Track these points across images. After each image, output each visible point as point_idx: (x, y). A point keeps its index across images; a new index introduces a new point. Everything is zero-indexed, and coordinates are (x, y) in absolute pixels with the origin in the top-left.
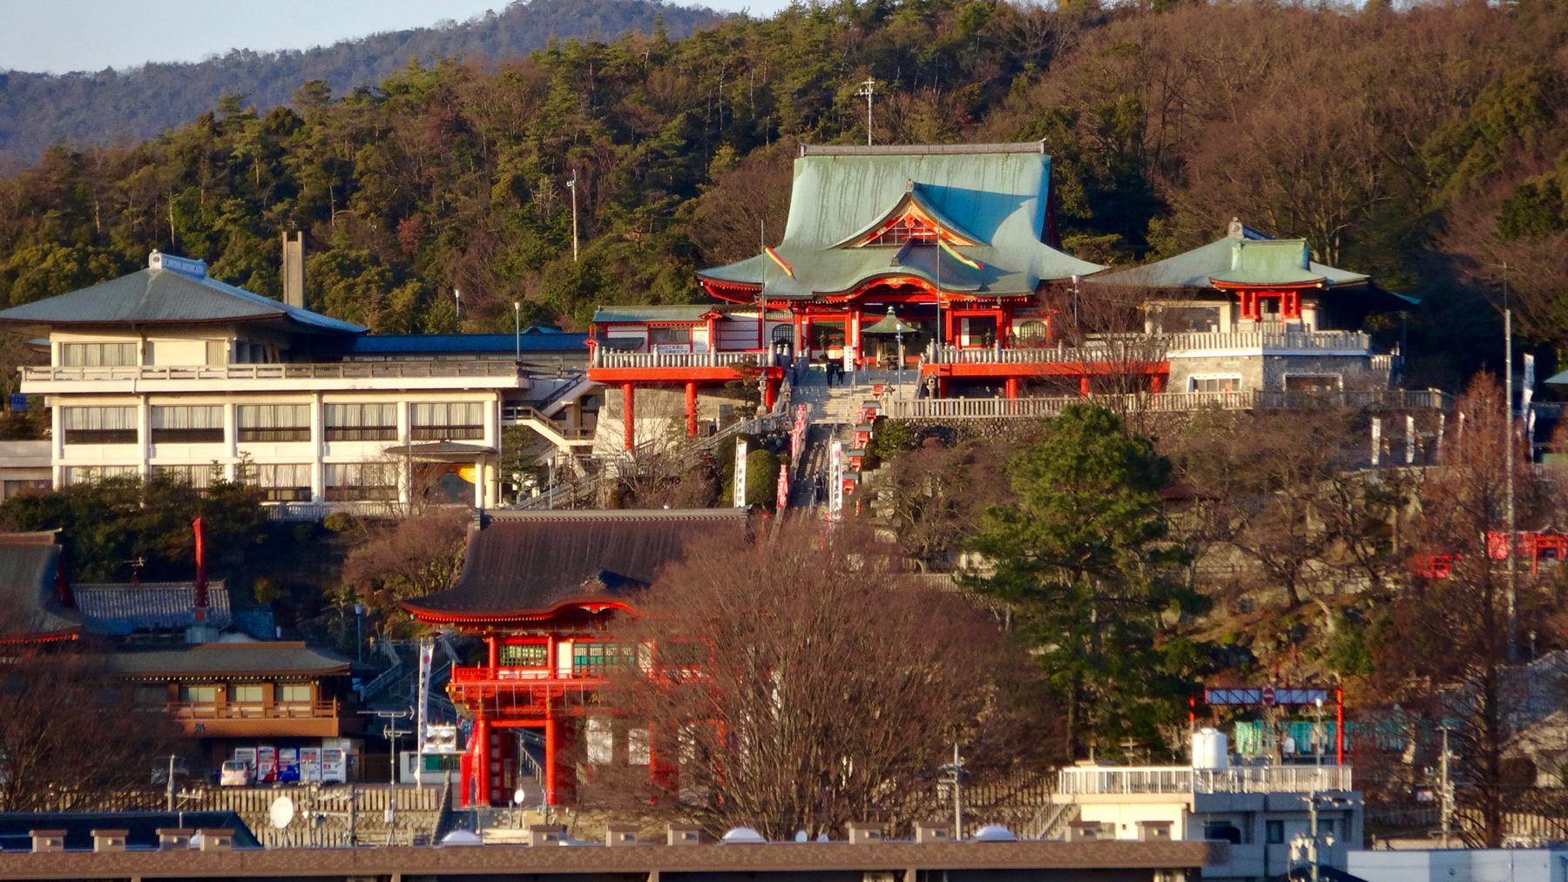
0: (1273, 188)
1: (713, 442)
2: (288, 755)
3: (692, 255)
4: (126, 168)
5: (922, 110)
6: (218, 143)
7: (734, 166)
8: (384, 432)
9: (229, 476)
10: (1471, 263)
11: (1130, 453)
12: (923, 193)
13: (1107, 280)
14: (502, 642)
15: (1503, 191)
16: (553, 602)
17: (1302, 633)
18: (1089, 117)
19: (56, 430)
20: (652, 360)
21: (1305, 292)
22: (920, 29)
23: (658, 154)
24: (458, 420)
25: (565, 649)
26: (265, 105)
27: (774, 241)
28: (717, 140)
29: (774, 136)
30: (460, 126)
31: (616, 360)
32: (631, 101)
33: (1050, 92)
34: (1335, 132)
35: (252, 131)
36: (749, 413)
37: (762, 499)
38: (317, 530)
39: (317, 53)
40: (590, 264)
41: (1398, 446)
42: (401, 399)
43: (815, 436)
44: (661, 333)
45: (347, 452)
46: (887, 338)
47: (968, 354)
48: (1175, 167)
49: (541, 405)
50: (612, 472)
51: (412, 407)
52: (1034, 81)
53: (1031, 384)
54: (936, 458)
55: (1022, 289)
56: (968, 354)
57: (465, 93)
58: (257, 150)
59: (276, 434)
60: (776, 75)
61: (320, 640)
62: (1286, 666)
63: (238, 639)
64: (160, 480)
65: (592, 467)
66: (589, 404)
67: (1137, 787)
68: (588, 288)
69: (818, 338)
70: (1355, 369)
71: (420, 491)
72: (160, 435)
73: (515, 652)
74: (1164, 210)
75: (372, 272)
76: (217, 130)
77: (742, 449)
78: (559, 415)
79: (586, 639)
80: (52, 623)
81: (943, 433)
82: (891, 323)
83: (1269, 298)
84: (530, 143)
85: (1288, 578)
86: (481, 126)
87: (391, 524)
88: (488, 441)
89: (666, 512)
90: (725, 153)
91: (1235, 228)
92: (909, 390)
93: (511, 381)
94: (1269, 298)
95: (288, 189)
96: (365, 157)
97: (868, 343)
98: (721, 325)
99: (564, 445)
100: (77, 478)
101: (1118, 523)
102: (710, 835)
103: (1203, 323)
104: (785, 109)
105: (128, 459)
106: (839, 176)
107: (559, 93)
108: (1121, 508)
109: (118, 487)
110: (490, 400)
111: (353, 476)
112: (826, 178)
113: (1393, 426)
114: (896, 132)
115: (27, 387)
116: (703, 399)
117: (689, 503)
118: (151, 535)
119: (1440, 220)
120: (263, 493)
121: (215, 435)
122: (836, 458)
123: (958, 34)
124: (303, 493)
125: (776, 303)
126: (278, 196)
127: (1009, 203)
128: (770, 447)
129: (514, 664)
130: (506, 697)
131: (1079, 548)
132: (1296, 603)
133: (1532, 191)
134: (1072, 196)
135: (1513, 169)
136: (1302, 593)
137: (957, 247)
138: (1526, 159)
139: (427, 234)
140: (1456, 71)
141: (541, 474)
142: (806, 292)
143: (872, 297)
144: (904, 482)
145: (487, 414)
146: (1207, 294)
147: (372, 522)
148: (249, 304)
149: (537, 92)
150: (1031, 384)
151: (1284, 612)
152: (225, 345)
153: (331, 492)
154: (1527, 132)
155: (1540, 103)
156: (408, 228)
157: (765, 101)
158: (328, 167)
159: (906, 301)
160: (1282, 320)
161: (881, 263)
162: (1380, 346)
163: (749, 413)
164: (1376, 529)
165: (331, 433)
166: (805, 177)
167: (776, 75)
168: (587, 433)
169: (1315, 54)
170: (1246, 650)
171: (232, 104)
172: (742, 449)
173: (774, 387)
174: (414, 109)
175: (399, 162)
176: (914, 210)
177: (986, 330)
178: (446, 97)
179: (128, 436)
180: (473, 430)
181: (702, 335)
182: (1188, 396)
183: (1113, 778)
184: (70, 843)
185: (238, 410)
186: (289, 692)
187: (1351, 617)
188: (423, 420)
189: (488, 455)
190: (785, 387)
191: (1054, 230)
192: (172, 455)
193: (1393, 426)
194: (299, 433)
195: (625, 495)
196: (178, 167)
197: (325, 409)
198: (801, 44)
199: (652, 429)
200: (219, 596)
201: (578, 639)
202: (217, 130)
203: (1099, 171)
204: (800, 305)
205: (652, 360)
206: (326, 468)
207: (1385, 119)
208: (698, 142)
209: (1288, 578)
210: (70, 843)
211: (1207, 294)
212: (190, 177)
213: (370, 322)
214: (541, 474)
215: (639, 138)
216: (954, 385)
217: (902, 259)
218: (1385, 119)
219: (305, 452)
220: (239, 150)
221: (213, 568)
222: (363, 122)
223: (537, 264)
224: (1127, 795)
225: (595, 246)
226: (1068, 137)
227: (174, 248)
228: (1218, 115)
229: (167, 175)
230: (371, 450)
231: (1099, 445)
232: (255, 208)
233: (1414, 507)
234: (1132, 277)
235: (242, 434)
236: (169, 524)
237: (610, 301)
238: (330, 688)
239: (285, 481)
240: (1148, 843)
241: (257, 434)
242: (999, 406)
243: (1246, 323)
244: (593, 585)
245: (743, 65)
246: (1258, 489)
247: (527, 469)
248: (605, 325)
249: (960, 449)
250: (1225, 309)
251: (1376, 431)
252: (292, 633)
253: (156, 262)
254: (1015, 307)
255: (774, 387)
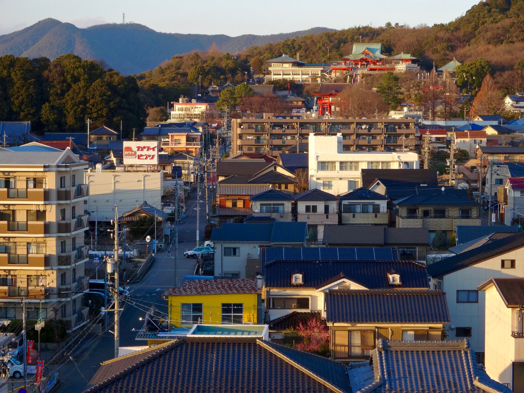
0: (406, 48)
1: (345, 76)
2: (299, 110)
3: (341, 55)
4: (276, 45)
5: (366, 39)
6: (287, 43)
7: (343, 46)
8: (308, 74)
9: (291, 79)
10: (428, 57)
11: (395, 77)
12: (368, 48)
13: (388, 58)
14: (323, 97)
15: (431, 49)
16: (329, 93)
17: (410, 97)
18: (385, 41)
19: (272, 74)
20: (338, 66)
21: (410, 60)
22: (364, 31)
23: (335, 44)
24: (316, 73)
25: (330, 98)
26: (291, 38)
27: (351, 54)
28: (341, 43)
29: (348, 42)
30: (313, 41)
31: (334, 67)
32: (332, 38)
33: (380, 37)
34: (413, 42)
35: (290, 41)
36: (349, 72)
37: (350, 81)
38: (301, 85)
39: (290, 33)
40: (330, 56)
41: (421, 77)
42: (310, 71)
43: (356, 75)
44: (338, 64)
45: (304, 77)
46: (364, 65)
47: (372, 66)
48: (394, 46)
49: (326, 72)
50: (334, 79)
51: (311, 72)
52: (377, 36)
53: (380, 69)
54: (370, 78)
55: (378, 59)
56: (372, 66)
57: (314, 37)
58: (291, 44)
59: (296, 74)
60: (348, 36)
61: (302, 97)
62: (409, 101)
63: (293, 97)
64: (284, 79)
65: (331, 78)
66: (331, 71)
67: (398, 114)
68: (330, 59)
69: (356, 64)
70: (416, 68)
71: (312, 81)
72: (284, 74)
73: (325, 98)
74: (393, 51)
75: (304, 57)
76: (286, 41)
77: (348, 76)
78: (327, 73)
79: (333, 97)
80: (274, 95)
81: (370, 75)
82: (364, 63)
83: (407, 60)
84: (321, 43)
85: (409, 91)
86: (315, 41)
87: (309, 84)
88: (320, 75)
89: (340, 83)
90: (342, 44)
91: (402, 53)
92: (366, 70)
93: (322, 69)
94: (407, 60)
95: (294, 48)
96: (303, 44)
97: (361, 65)
98: (345, 63)
99: (328, 76)
100: (275, 79)
101: (393, 85)
102: (361, 118)
103: (399, 63)
104: (349, 40)
105: (280, 77)
106: (358, 46)
107: (324, 38)
108: (394, 83)
109: (279, 80)
110: (320, 71)
111: (305, 79)
112: (357, 47)
113: (421, 75)
114: (363, 42)
115: (269, 69)
116: (344, 71)
117: (342, 82)
118: (283, 85)
119: (424, 51)
120: (295, 81)
121: (290, 75)
122: (359, 78)
123: (368, 31)
124: (299, 81)
125: (352, 60)
126: (293, 49)
127: (377, 50)
128: (351, 76)
129: (325, 100)
130: (324, 103)
131: (389, 88)
132: (410, 94)
133: (435, 49)
134: (383, 49)
135: (432, 46)
136: (410, 93)
137: (371, 54)
138: (434, 45)
139: (310, 53)
140: (425, 35)
141: (325, 79)
142: (355, 59)
143: (362, 60)
144: (366, 80)
145: (320, 73)
146: (400, 60)
147: (307, 84)
148: (294, 60)
149: (322, 37)
150: (380, 69)
151: (408, 95)
152: (291, 64)
153: (302, 81)
154: (434, 42)
155: (435, 39)
156: (307, 52)
157: (347, 38)
158: (299, 45)
159: (366, 60)
160: (408, 63)
161: (363, 56)
162: (418, 66)
163: (349, 72)
164: (418, 86)
165: (302, 74)
166: (355, 47)
167: (348, 36)
168: (331, 75)
169: (410, 34)
170: (404, 99)
171: (288, 39)
172: (348, 76)
173: (351, 70)
174: (308, 39)
175: (306, 45)
176: (367, 50)
177: (375, 63)
178: (312, 38)
179: (280, 75)
180: (318, 74)
181: (343, 64)
182: (398, 71)
183: (395, 113)
184: (298, 118)
185: (292, 72)
186: (299, 103)
187: (416, 96)
188: (312, 73)
189: (320, 77)
190: (353, 70)
191: (382, 53)
192: (285, 77)
193: (421, 75)
194: (299, 74)
195: (335, 81)
196: (282, 45)
197: (302, 72)
198: (351, 32)
199: (338, 74)
200: (291, 92)
201: (332, 97)
202: (286, 41)
203: (386, 46)
204: (354, 61)
205: (338, 66)
206: (302, 78)
207: (418, 41)
208: (339, 43)
209: (409, 91)
210: (298, 118)
211: (400, 60)
212: (284, 46)
213: (306, 62)
214: (325, 79)
215: (333, 42)
216: (371, 70)
217: (365, 56)
218: (418, 41)
219: (300, 76)
220: (289, 43)
221: (290, 89)
222: (303, 40)
223: (323, 56)
224: (397, 115)
225: (330, 54)
226: (383, 42)
227: (286, 54)
228: (399, 40)
229: (281, 46)
230: (307, 76)
231: (391, 76)
232: (291, 50)
233: (423, 83)
234: (391, 58)
235: (293, 74)
236: (285, 84)
237: (332, 60)
238: (303, 102)
239: (297, 80)
240: (401, 119)
241: (294, 74)
242: (376, 72)
243: (404, 63)
244: (334, 91)
245: (344, 35)
246: (405, 81)
247: (324, 79)
248: (332, 63)
249: (372, 77)
250: (401, 62)
251: (419, 75)
252: (298, 96)
253: (283, 55)
254: (378, 61)
255: (351, 70)
